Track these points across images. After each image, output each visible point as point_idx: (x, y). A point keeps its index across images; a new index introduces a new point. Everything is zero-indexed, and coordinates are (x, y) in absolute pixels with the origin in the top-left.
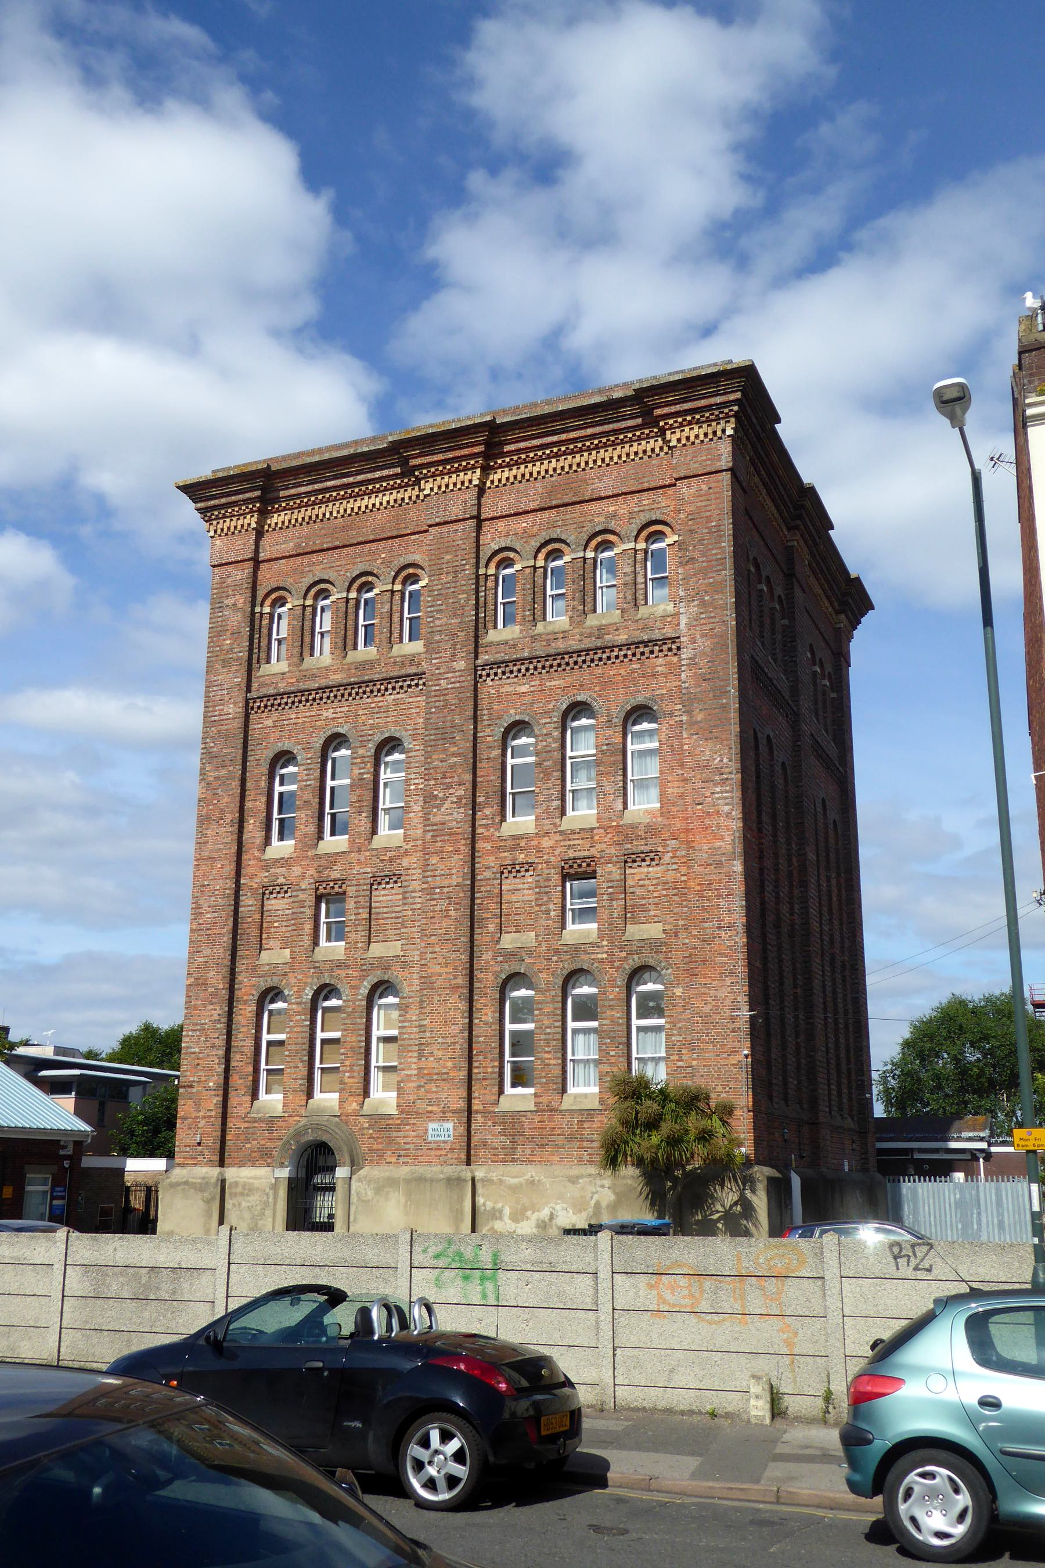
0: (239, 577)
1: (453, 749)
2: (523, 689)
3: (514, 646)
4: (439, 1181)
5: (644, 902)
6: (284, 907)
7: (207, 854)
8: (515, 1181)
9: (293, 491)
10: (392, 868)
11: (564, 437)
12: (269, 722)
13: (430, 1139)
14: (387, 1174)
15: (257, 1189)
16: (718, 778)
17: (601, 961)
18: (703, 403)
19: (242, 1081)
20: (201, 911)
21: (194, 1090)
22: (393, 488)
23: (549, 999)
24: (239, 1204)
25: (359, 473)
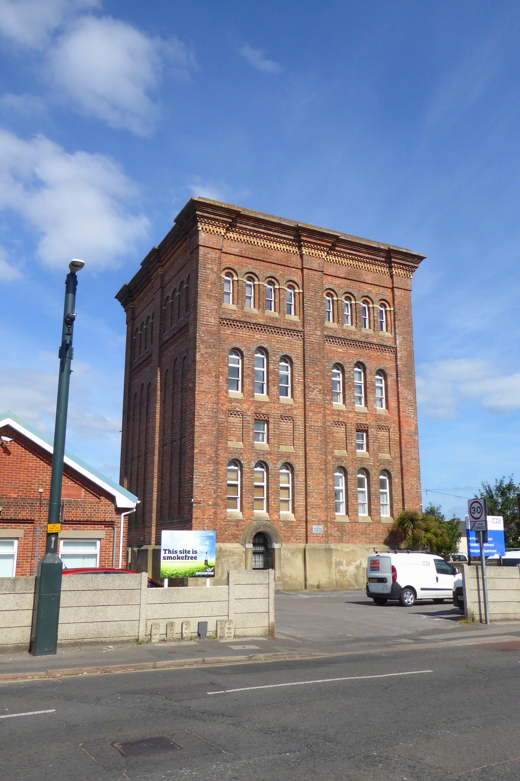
0: (214, 256)
1: (317, 368)
2: (340, 350)
3: (336, 331)
4: (322, 550)
5: (383, 445)
6: (237, 422)
7: (203, 389)
8: (347, 550)
9: (244, 226)
10: (290, 414)
11: (358, 253)
12: (228, 332)
13: (314, 532)
14: (295, 547)
15: (236, 553)
16: (410, 404)
17: (371, 465)
18: (407, 263)
19: (221, 502)
20: (200, 417)
21: (202, 505)
22: (287, 244)
23: (353, 478)
24: (228, 560)
25: (276, 231)
